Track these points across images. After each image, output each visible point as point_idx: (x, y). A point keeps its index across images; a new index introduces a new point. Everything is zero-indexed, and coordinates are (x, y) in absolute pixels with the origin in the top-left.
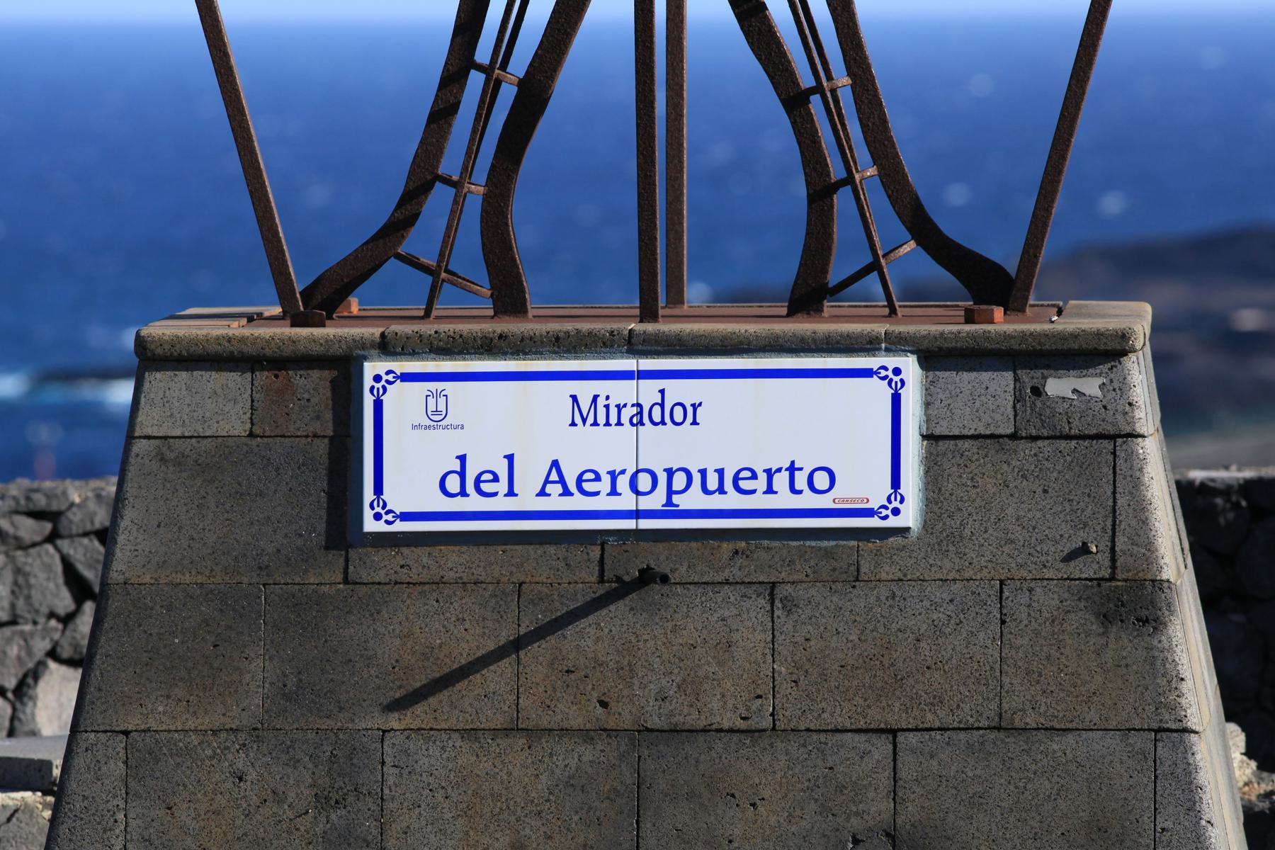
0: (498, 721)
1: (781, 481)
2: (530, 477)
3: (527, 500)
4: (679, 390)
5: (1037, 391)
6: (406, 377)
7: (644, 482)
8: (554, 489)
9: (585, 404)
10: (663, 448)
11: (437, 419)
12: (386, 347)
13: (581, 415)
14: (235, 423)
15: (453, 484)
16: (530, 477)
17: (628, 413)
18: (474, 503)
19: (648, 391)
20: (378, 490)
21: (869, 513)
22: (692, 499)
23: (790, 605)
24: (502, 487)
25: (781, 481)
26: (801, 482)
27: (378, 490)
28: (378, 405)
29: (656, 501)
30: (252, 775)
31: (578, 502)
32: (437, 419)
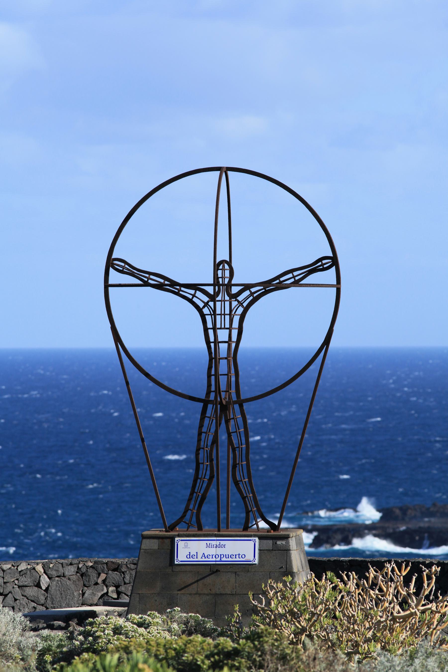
0: (195, 592)
1: (237, 556)
2: (200, 556)
3: (199, 559)
4: (222, 543)
5: (276, 543)
6: (182, 540)
7: (217, 556)
8: (203, 557)
9: (208, 544)
10: (220, 551)
11: (186, 547)
12: (179, 536)
13: (208, 546)
14: (156, 547)
15: (188, 556)
16: (200, 556)
17: (214, 546)
18: (191, 559)
19: (218, 543)
20: (177, 557)
21: (250, 561)
22: (224, 559)
23: (238, 575)
25: (237, 556)
26: (240, 556)
27: (177, 557)
28: (177, 545)
29: (219, 559)
30: (158, 600)
31: (207, 559)
32: (186, 547)
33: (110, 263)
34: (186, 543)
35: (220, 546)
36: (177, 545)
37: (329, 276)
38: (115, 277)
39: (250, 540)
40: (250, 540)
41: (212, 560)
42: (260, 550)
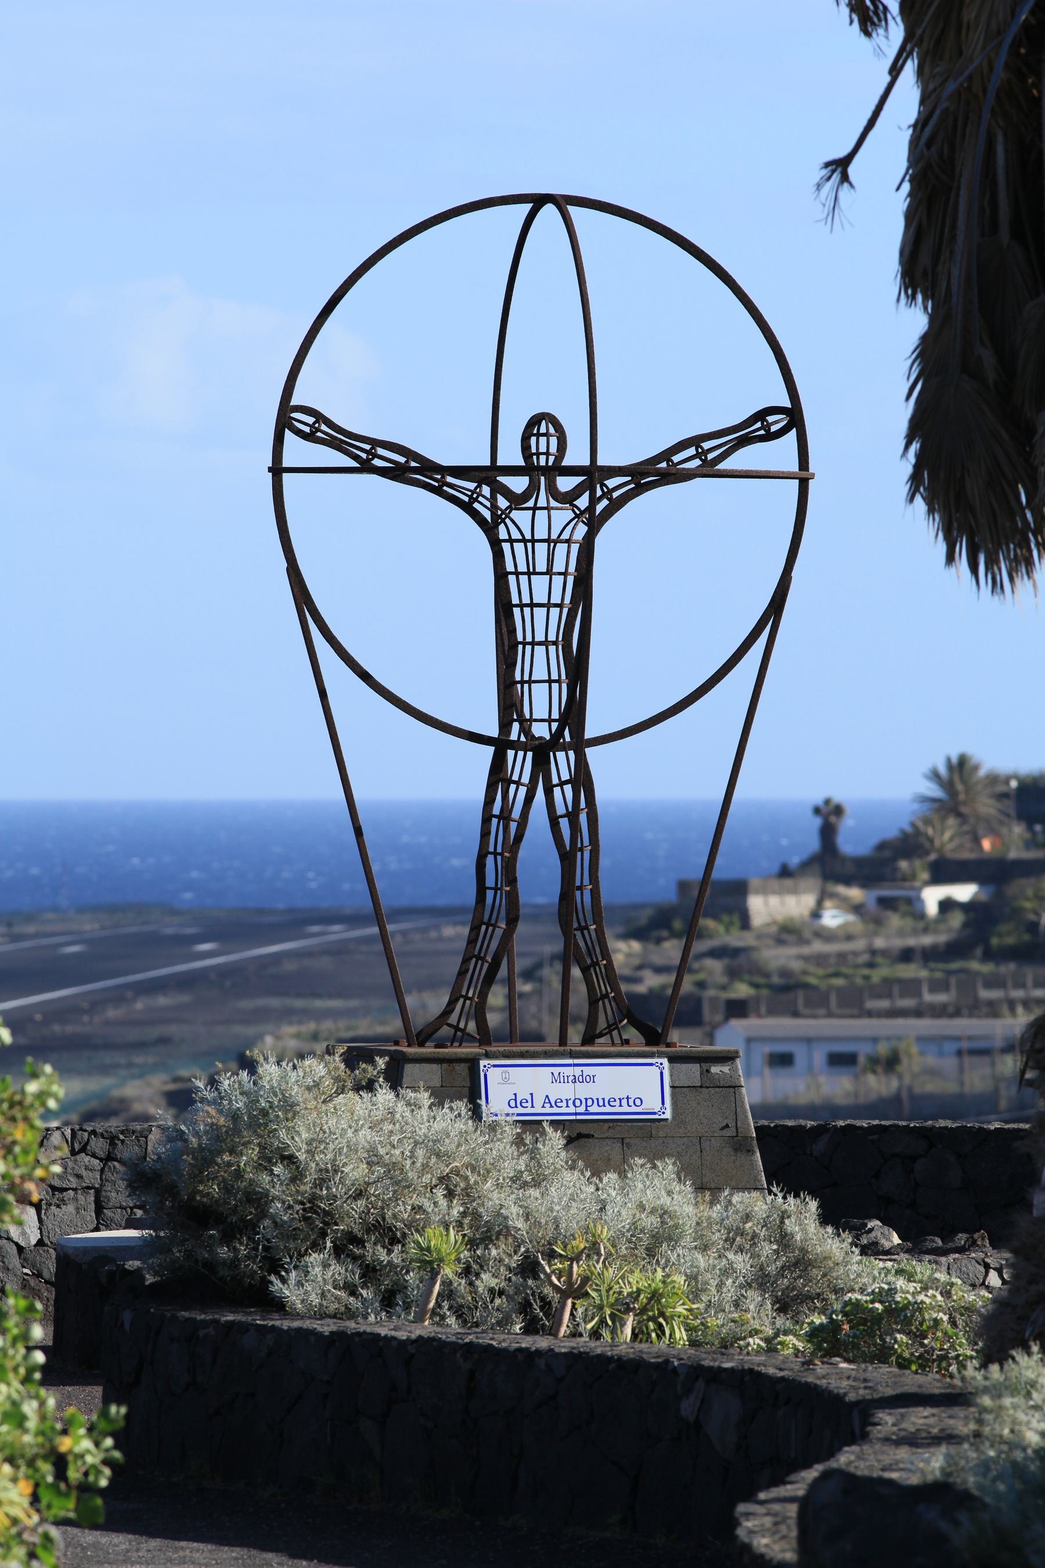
2: (539, 1101)
4: (587, 1070)
5: (708, 1071)
6: (494, 1066)
7: (578, 1103)
8: (547, 1105)
9: (556, 1075)
10: (584, 1091)
13: (555, 1079)
15: (513, 1103)
16: (539, 1101)
19: (578, 1071)
21: (654, 1113)
22: (594, 1109)
23: (629, 1146)
24: (529, 1104)
26: (631, 1102)
29: (582, 1109)
31: (555, 1110)
32: (506, 1081)
34: (506, 1072)
36: (485, 1076)
38: (298, 451)
39: (651, 1064)
40: (651, 1064)
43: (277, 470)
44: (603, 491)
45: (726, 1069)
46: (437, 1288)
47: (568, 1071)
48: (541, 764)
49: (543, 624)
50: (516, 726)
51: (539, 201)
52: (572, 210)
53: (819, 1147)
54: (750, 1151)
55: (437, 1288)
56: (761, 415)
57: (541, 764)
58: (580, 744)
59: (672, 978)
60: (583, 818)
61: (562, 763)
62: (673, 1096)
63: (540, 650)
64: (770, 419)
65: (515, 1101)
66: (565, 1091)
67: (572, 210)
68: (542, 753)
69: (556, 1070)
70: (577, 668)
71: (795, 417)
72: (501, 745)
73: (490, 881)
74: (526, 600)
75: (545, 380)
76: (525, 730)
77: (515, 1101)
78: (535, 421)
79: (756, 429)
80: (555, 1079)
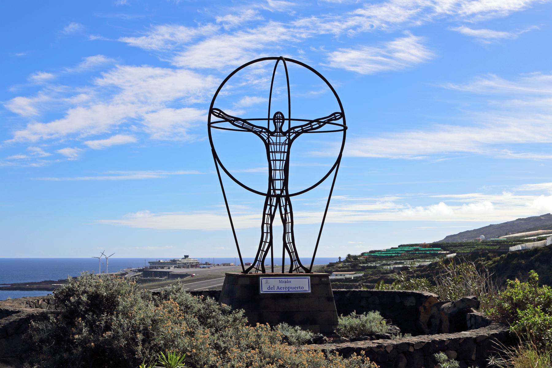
2: (276, 288)
4: (49, 137)
10: (288, 285)
11: (267, 283)
13: (280, 282)
16: (276, 288)
19: (286, 280)
32: (267, 283)
33: (211, 111)
35: (288, 282)
37: (341, 121)
38: (214, 118)
41: (283, 291)
42: (311, 284)
43: (209, 124)
44: (293, 134)
45: (326, 279)
46: (342, 42)
47: (284, 280)
48: (278, 201)
49: (279, 165)
50: (272, 191)
51: (279, 59)
52: (286, 62)
53: (348, 295)
54: (332, 301)
55: (342, 42)
56: (334, 114)
57: (278, 201)
58: (287, 197)
59: (213, 83)
60: (283, 212)
61: (283, 200)
62: (311, 287)
63: (278, 168)
64: (336, 115)
65: (269, 288)
66: (283, 285)
67: (286, 62)
68: (278, 197)
69: (280, 280)
70: (286, 170)
71: (342, 115)
72: (268, 196)
73: (265, 230)
74: (273, 150)
75: (279, 105)
76: (274, 192)
77: (269, 288)
78: (277, 113)
79: (329, 120)
80: (280, 282)
